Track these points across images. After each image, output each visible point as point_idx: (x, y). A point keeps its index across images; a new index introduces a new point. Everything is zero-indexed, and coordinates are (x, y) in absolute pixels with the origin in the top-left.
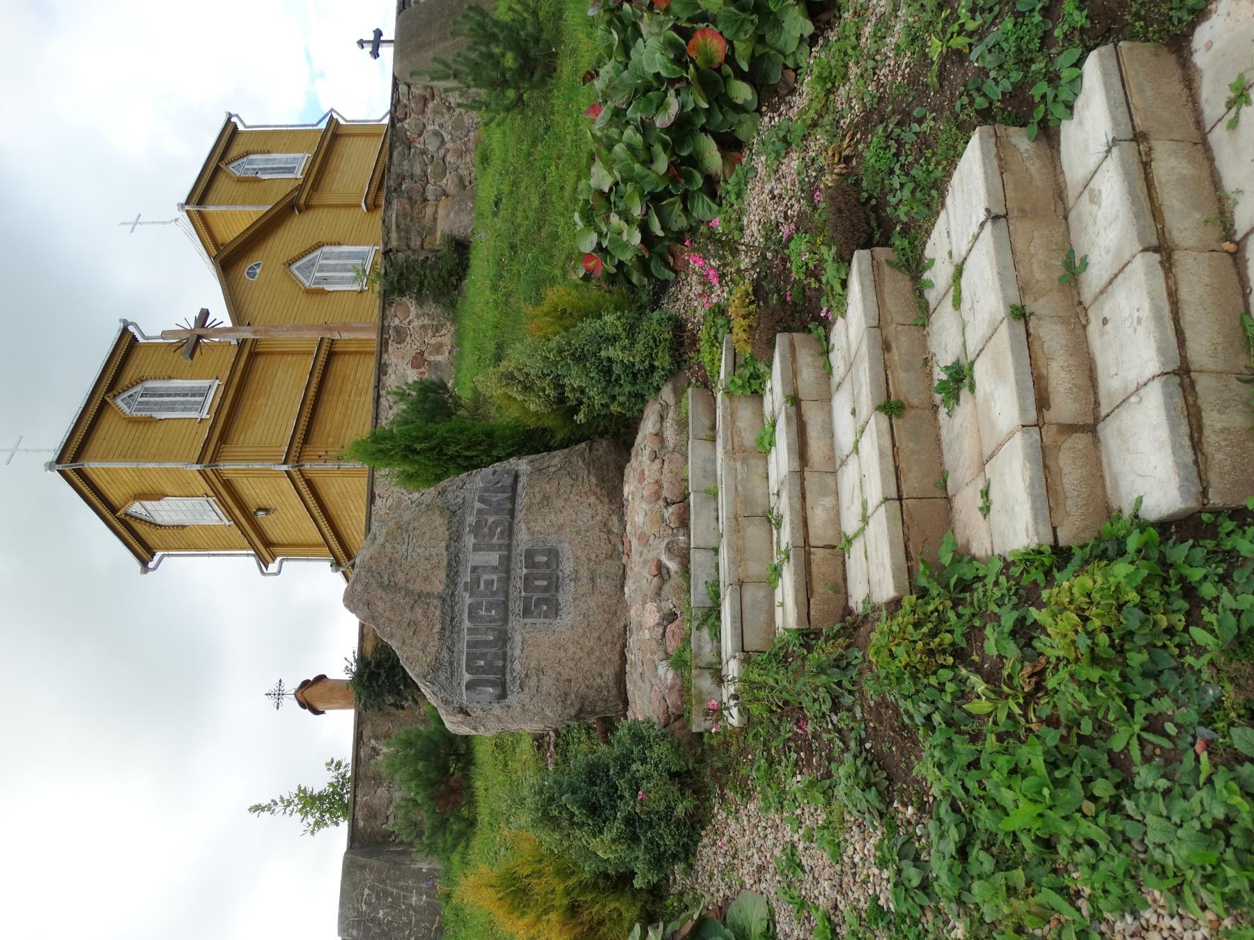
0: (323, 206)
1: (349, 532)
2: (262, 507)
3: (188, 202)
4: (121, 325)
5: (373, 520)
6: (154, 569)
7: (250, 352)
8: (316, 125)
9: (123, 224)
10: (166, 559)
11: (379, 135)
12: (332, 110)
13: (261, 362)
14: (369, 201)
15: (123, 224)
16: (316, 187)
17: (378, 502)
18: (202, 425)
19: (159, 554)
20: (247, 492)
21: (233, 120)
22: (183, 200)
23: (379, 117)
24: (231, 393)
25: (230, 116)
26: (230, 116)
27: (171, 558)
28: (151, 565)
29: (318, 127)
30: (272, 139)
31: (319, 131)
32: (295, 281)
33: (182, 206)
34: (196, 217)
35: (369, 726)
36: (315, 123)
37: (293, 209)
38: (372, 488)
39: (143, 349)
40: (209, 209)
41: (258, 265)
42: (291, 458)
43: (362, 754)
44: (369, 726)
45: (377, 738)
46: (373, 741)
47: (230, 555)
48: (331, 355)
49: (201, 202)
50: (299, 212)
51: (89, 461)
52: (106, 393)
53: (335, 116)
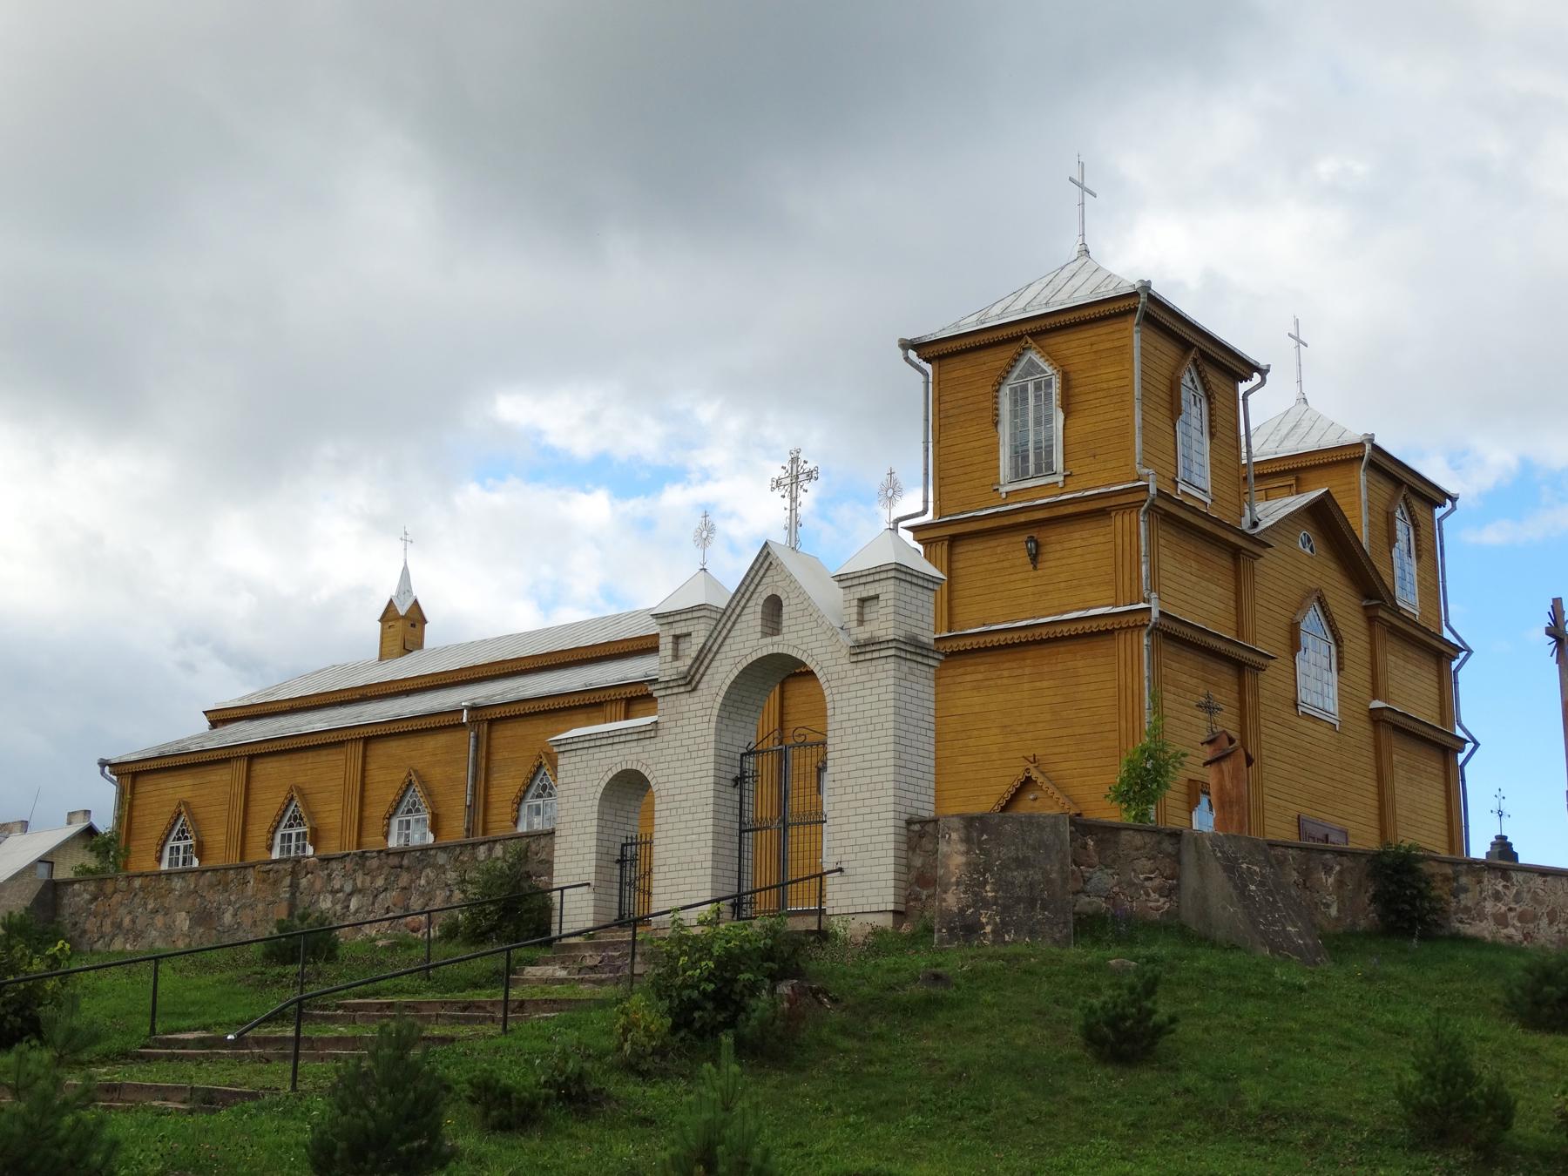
0: (1372, 643)
1: (982, 668)
2: (1043, 550)
3: (1376, 448)
4: (1262, 363)
5: (1525, 874)
6: (907, 359)
7: (1241, 548)
8: (1447, 625)
9: (1297, 322)
10: (921, 377)
11: (1239, 633)
12: (1470, 652)
13: (1225, 562)
14: (1386, 713)
15: (1297, 322)
16: (1394, 631)
17: (1540, 880)
18: (1170, 483)
19: (928, 367)
20: (1076, 535)
21: (1257, 377)
22: (1377, 441)
23: (1464, 722)
24: (1208, 526)
25: (1263, 372)
26: (1263, 372)
27: (922, 386)
28: (912, 354)
29: (1445, 628)
30: (1428, 552)
31: (1441, 630)
32: (1301, 607)
33: (1371, 439)
34: (1357, 453)
35: (1351, 864)
36: (1451, 623)
37: (1368, 596)
38: (1552, 875)
39: (1232, 386)
40: (1362, 476)
41: (1311, 549)
42: (1166, 622)
43: (1328, 856)
44: (1351, 864)
45: (1341, 873)
46: (1338, 868)
47: (926, 474)
48: (1239, 666)
49: (1373, 466)
50: (1365, 608)
51: (1141, 331)
52: (1200, 350)
53: (1462, 655)
